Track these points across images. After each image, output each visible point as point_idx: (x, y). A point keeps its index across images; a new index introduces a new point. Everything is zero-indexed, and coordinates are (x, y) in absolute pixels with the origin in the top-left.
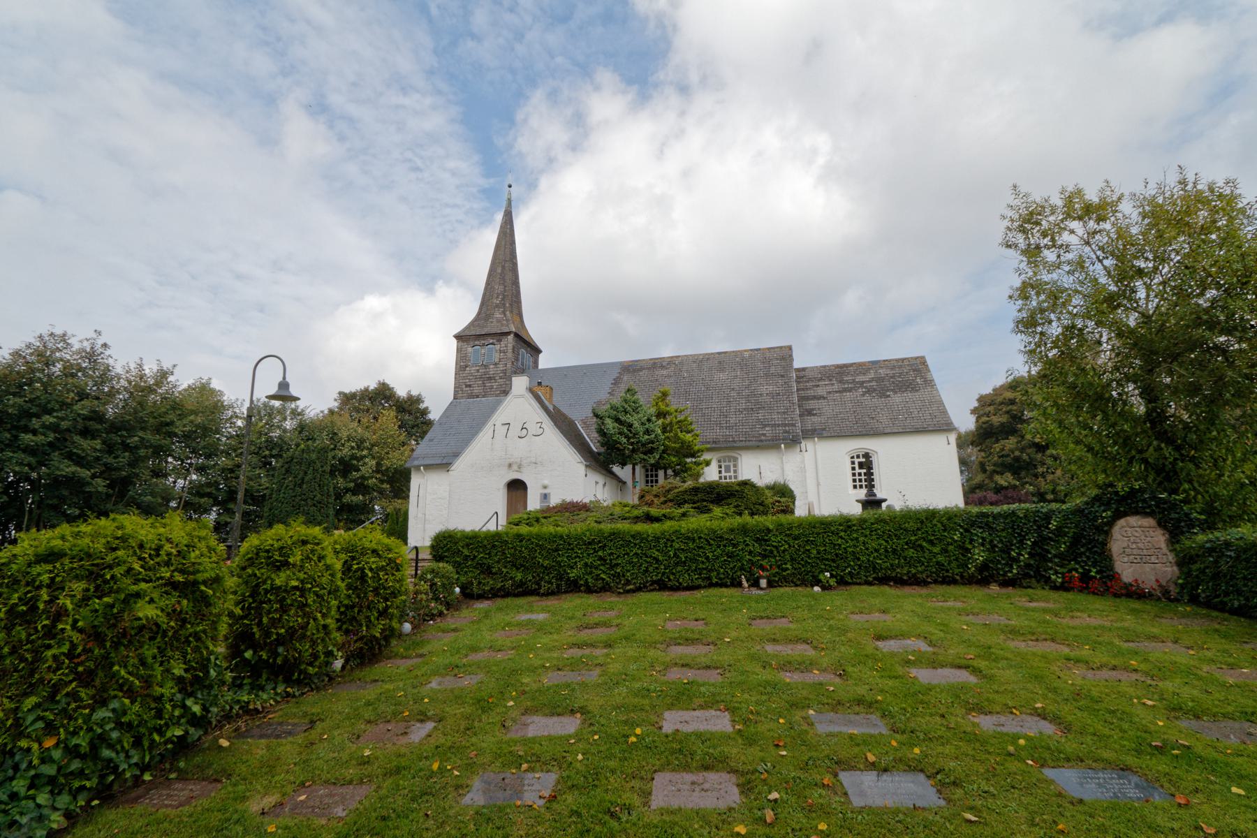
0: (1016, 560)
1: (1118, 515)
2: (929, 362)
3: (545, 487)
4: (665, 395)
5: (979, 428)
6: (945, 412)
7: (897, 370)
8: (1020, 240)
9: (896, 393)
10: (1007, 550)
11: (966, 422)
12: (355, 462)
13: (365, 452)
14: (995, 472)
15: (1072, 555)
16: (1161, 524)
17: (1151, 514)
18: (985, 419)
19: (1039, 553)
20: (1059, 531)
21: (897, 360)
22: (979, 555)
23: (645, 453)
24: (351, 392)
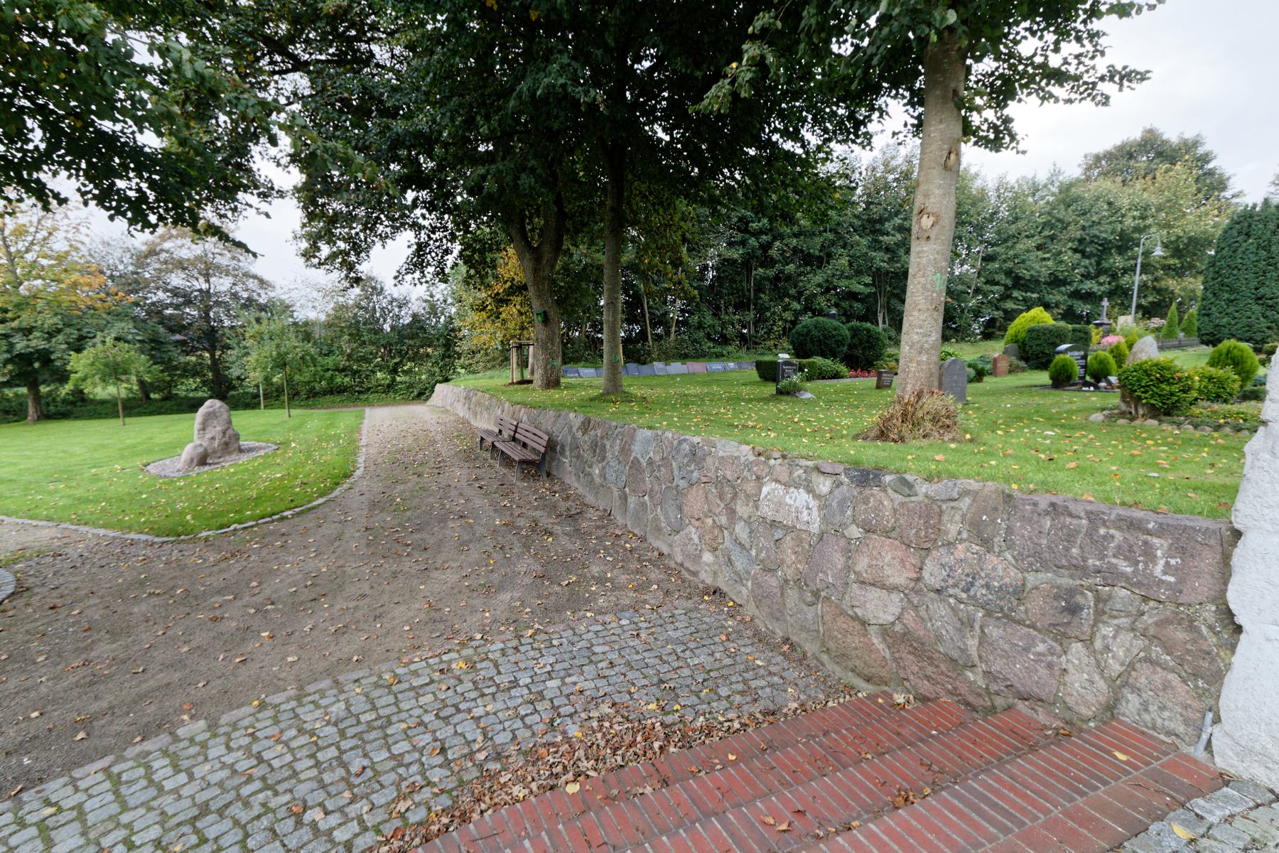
13: (1150, 221)
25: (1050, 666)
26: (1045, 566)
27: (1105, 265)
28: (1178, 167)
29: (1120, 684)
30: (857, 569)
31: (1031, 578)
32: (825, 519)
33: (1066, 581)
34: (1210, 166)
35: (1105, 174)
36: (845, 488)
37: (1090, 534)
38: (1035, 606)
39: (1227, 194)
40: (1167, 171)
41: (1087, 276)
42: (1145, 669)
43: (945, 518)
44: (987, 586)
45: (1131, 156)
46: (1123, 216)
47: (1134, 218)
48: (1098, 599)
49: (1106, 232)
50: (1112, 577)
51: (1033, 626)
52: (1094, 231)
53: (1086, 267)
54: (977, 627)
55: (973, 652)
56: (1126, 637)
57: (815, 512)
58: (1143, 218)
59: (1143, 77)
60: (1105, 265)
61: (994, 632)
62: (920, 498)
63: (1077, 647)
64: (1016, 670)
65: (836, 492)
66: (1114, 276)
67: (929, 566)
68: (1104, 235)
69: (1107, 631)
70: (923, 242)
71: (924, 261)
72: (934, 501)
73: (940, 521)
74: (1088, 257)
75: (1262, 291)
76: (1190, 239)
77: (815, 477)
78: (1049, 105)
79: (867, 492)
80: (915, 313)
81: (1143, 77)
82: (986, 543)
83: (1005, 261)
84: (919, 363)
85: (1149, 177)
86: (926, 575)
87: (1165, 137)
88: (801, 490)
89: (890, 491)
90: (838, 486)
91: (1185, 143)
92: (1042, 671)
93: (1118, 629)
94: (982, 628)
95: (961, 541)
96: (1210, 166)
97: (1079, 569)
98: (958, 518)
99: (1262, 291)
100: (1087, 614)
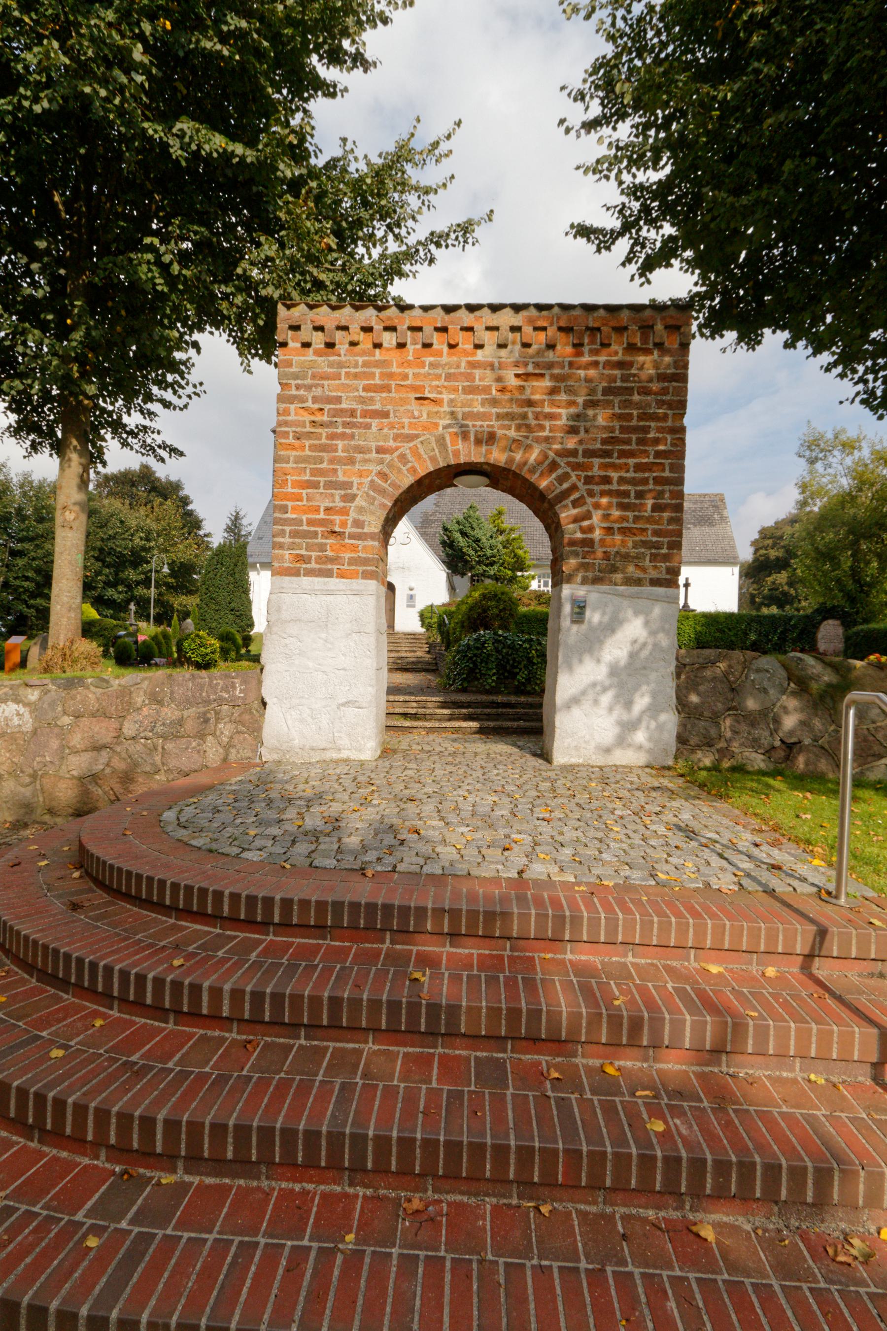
0: (770, 641)
1: (825, 619)
2: (727, 500)
3: (411, 589)
4: (500, 513)
5: (756, 560)
6: (733, 547)
7: (699, 505)
8: (807, 453)
9: (695, 526)
10: (767, 636)
11: (746, 554)
12: (143, 554)
13: (152, 544)
14: (762, 604)
15: (799, 638)
16: (843, 624)
17: (837, 619)
18: (763, 552)
19: (783, 638)
20: (795, 627)
21: (700, 495)
22: (753, 637)
23: (487, 565)
24: (120, 472)
25: (199, 752)
26: (191, 706)
27: (121, 575)
28: (169, 502)
29: (227, 747)
30: (71, 744)
31: (186, 713)
32: (36, 719)
33: (202, 710)
34: (189, 508)
35: (111, 494)
36: (53, 693)
37: (210, 685)
38: (190, 726)
39: (201, 533)
40: (161, 504)
41: (108, 584)
42: (236, 736)
43: (134, 695)
44: (164, 724)
45: (133, 484)
46: (132, 535)
47: (141, 538)
48: (217, 713)
49: (120, 546)
50: (220, 701)
51: (189, 736)
52: (110, 544)
53: (107, 576)
54: (160, 749)
55: (159, 763)
56: (229, 726)
57: (27, 716)
58: (148, 540)
59: (182, 454)
60: (121, 575)
61: (169, 746)
62: (115, 687)
63: (210, 738)
64: (184, 762)
65: (46, 698)
66: (129, 587)
67: (126, 725)
68: (118, 549)
69: (221, 726)
70: (67, 529)
71: (69, 543)
72: (125, 687)
73: (130, 698)
74: (108, 567)
75: (233, 605)
76: (181, 563)
77: (22, 691)
78: (126, 450)
79: (74, 692)
80: (64, 581)
81: (182, 454)
82: (160, 703)
83: (34, 559)
84: (69, 618)
85: (149, 506)
86: (125, 731)
87: (157, 475)
88: (9, 703)
89: (92, 688)
90: (46, 694)
91: (170, 483)
92: (196, 756)
93: (225, 724)
94: (163, 748)
95: (145, 705)
96: (189, 508)
97: (207, 702)
98: (142, 693)
99: (233, 605)
100: (212, 721)
